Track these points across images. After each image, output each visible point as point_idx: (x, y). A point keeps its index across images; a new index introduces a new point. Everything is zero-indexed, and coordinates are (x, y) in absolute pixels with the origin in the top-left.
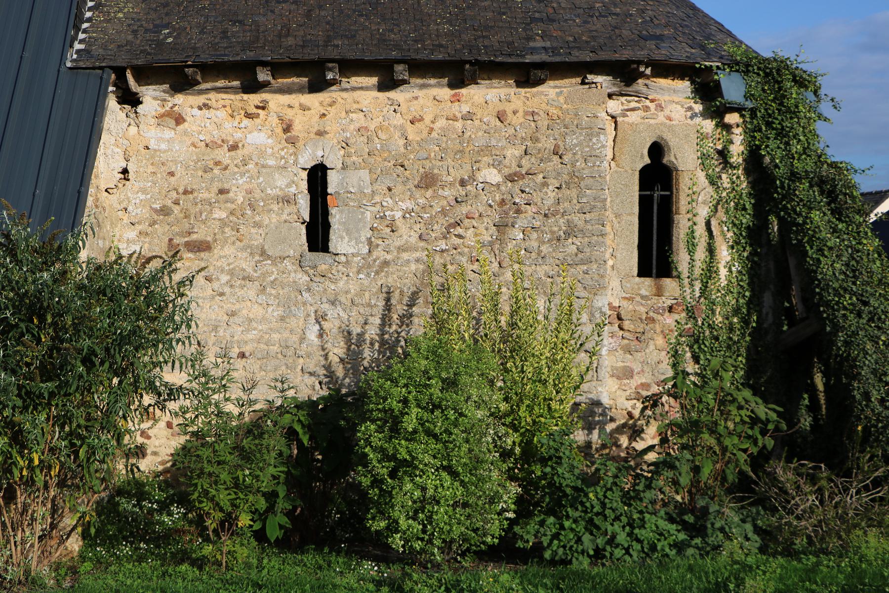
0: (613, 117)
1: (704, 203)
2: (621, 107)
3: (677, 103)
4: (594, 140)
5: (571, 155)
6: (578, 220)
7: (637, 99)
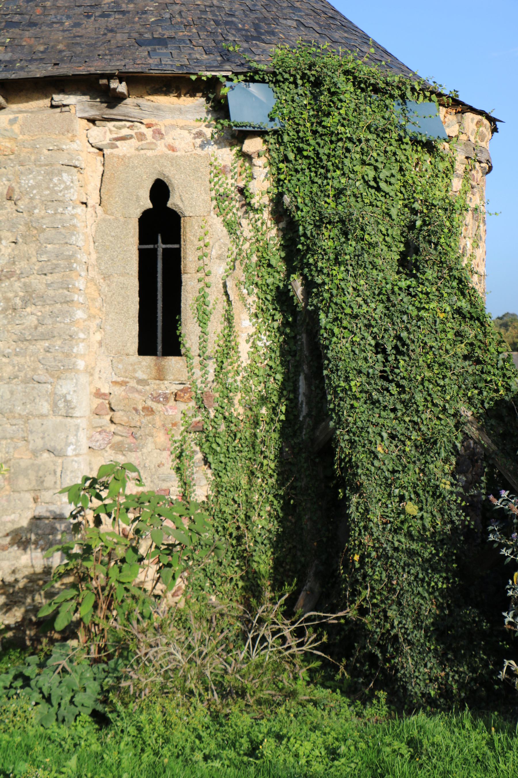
0: (101, 150)
1: (220, 257)
2: (109, 136)
3: (182, 128)
4: (55, 180)
5: (27, 200)
6: (37, 282)
7: (128, 124)
